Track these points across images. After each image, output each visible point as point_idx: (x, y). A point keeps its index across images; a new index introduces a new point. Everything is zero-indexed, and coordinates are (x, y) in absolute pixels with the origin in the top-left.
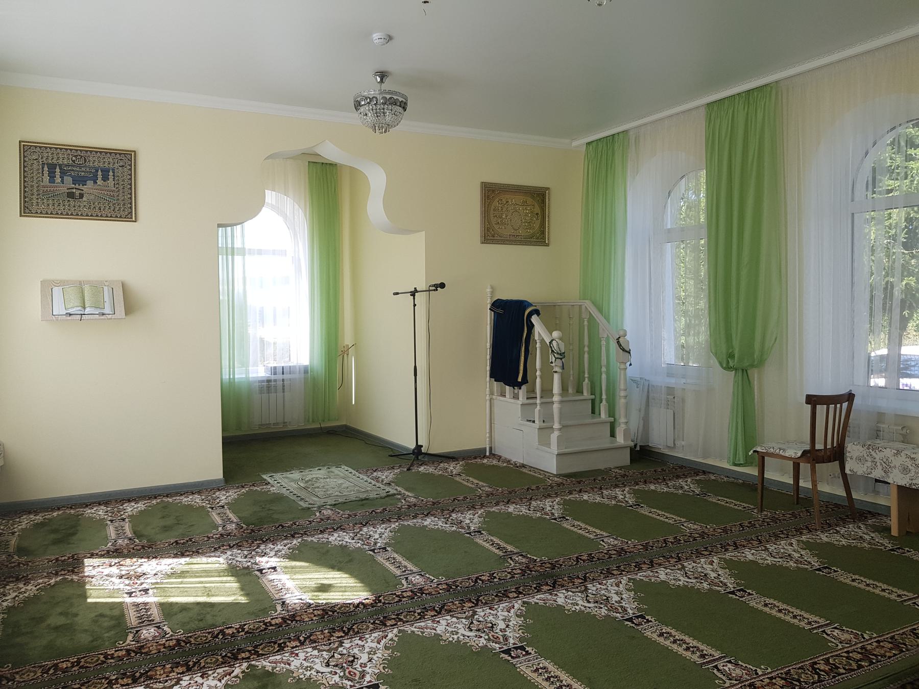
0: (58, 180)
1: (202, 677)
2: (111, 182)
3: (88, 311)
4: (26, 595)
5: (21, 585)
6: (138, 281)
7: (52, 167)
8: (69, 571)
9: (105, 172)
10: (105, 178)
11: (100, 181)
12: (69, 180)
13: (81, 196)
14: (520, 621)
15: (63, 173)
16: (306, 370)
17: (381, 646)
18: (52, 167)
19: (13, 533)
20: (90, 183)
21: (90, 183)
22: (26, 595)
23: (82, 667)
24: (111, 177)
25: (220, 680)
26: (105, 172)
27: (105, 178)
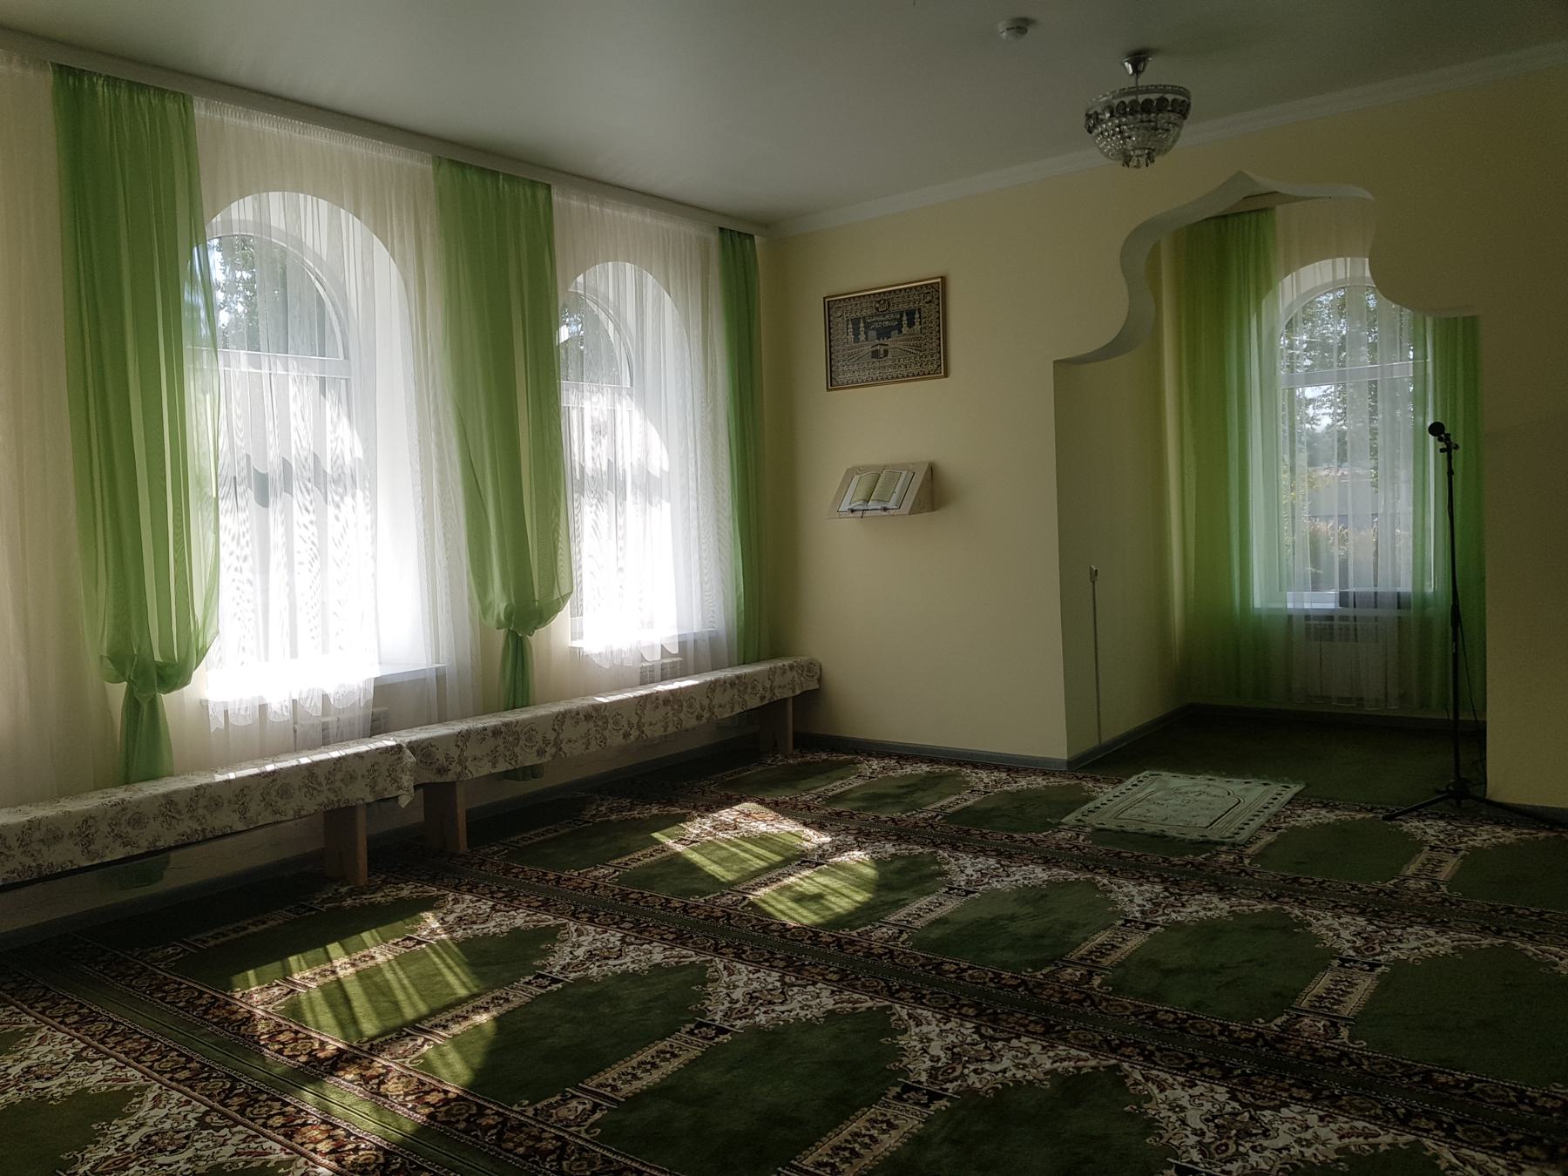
0: (862, 337)
1: (1321, 1119)
2: (917, 327)
3: (871, 505)
4: (1432, 950)
5: (1431, 932)
6: (952, 460)
7: (856, 322)
8: (1523, 935)
9: (911, 314)
10: (911, 324)
11: (905, 330)
12: (873, 334)
13: (886, 352)
14: (902, 1041)
15: (867, 326)
16: (1400, 601)
17: (1336, 1142)
18: (856, 322)
19: (1456, 851)
20: (894, 333)
21: (894, 333)
22: (1432, 950)
23: (1472, 1096)
24: (917, 320)
25: (1341, 1137)
26: (911, 314)
27: (911, 324)
